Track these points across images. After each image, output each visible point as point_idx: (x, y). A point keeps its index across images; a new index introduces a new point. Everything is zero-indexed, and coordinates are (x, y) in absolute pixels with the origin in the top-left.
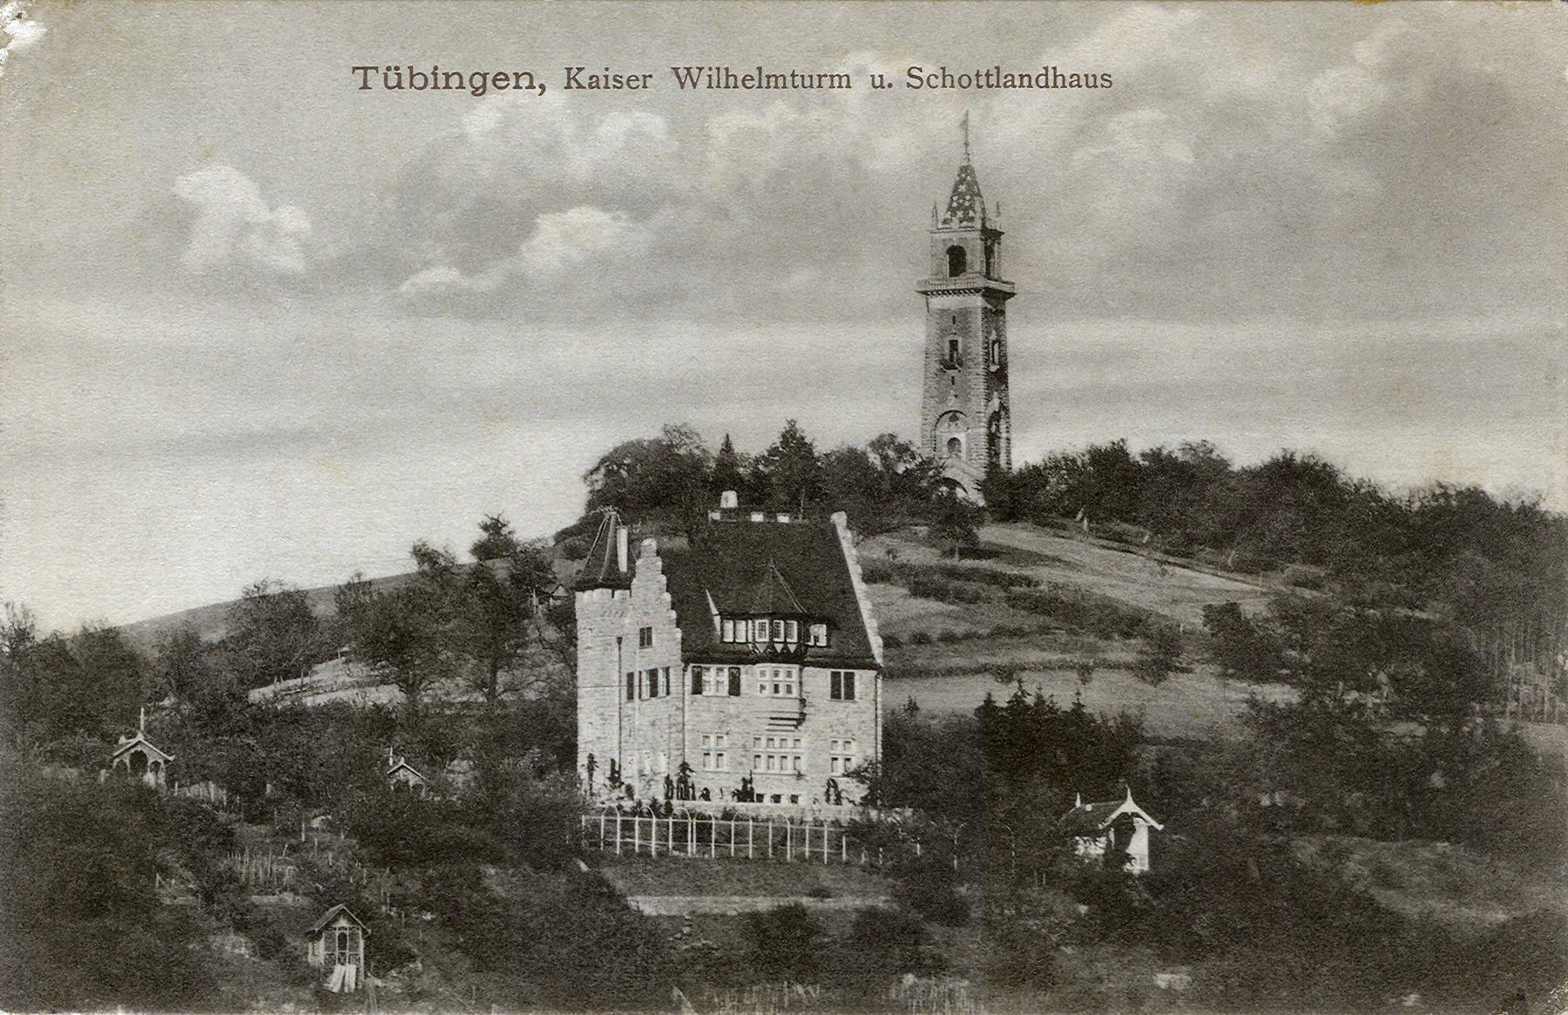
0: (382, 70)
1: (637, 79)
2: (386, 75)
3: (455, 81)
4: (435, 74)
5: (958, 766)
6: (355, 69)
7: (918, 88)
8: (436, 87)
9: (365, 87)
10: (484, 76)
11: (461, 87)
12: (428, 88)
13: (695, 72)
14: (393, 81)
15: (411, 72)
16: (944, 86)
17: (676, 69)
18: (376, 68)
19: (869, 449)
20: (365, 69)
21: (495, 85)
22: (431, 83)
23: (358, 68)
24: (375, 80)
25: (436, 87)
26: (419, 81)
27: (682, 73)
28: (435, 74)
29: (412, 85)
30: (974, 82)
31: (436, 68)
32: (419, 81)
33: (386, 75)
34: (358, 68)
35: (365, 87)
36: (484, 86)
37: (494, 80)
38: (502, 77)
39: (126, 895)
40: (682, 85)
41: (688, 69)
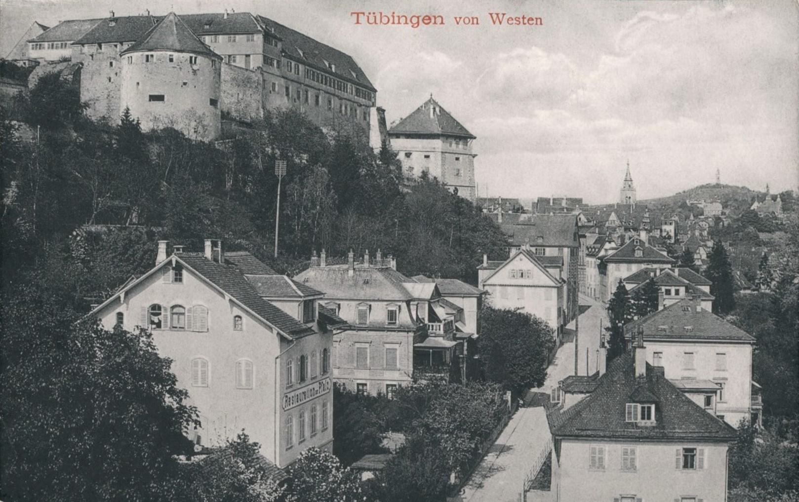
0: (367, 14)
1: (533, 20)
2: (368, 17)
3: (403, 20)
4: (393, 17)
5: (673, 211)
6: (352, 13)
7: (368, 22)
8: (393, 23)
9: (358, 23)
10: (418, 17)
11: (406, 23)
12: (390, 23)
13: (501, 16)
14: (372, 20)
15: (381, 15)
16: (537, 24)
17: (491, 14)
18: (364, 13)
19: (779, 196)
20: (358, 14)
21: (424, 23)
22: (391, 21)
23: (354, 13)
24: (362, 19)
25: (393, 23)
26: (385, 20)
27: (495, 16)
28: (393, 17)
29: (381, 21)
30: (391, 21)
31: (394, 13)
32: (385, 20)
33: (368, 17)
34: (354, 13)
35: (358, 23)
36: (418, 22)
37: (423, 20)
38: (427, 18)
39: (793, 371)
40: (494, 23)
41: (497, 14)
